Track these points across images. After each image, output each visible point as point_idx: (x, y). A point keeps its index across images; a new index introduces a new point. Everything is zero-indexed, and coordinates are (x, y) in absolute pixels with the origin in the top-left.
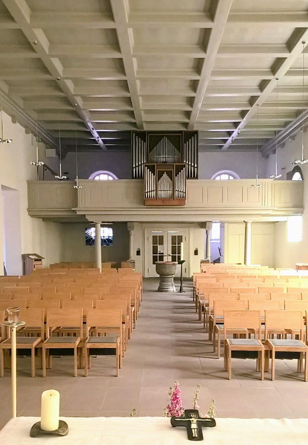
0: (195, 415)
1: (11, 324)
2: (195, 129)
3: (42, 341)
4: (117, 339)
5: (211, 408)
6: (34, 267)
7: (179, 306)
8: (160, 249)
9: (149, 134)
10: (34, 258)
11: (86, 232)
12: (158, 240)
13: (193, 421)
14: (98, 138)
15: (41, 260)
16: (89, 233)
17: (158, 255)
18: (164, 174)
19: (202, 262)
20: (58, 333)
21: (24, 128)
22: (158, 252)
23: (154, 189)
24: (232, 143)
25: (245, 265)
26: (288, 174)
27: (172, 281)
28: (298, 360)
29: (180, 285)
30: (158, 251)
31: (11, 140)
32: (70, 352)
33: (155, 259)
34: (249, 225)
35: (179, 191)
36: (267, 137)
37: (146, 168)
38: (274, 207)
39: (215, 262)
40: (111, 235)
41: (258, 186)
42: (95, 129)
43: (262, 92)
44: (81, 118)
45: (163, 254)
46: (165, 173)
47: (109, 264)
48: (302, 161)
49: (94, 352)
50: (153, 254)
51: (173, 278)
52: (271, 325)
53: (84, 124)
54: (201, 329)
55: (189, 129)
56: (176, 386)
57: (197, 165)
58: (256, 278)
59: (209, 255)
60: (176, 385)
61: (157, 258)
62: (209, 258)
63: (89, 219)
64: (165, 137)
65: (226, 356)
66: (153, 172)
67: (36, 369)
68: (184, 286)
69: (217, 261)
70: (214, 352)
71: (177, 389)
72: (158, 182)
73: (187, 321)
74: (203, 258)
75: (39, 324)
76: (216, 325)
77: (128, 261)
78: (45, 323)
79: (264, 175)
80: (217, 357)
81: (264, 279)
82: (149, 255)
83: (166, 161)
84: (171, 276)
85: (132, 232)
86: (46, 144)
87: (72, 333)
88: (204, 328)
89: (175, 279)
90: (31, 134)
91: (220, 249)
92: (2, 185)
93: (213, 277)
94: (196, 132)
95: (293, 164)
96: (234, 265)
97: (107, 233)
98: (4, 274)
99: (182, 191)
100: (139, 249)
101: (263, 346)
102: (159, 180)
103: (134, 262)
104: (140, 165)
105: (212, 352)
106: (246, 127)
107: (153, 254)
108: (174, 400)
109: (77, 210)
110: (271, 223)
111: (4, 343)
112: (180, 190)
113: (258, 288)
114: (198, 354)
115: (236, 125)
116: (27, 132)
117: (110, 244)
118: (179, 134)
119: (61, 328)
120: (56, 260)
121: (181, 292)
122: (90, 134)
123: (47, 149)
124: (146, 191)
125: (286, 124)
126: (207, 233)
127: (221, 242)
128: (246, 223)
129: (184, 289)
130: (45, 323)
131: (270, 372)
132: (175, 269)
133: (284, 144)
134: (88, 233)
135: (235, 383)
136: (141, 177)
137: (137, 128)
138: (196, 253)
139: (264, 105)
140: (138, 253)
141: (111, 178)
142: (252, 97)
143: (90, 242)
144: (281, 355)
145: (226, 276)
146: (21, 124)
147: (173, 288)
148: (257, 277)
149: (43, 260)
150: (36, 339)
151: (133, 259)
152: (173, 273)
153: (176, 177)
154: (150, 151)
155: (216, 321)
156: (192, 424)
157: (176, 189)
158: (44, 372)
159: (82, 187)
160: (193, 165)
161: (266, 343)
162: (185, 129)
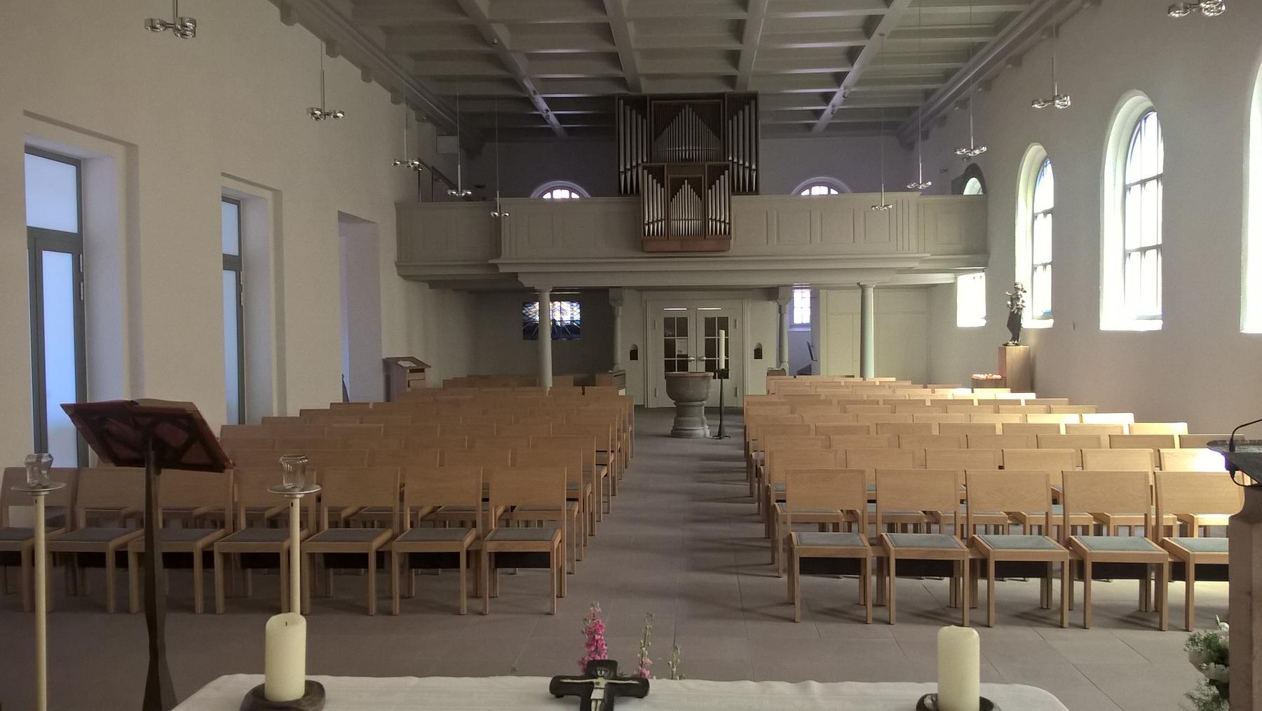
0: (606, 671)
1: (289, 490)
2: (751, 88)
3: (393, 537)
4: (555, 532)
5: (671, 663)
6: (409, 386)
7: (710, 467)
8: (679, 346)
9: (652, 102)
10: (408, 366)
11: (524, 311)
12: (677, 327)
13: (598, 683)
14: (547, 111)
15: (422, 371)
16: (530, 313)
17: (676, 359)
18: (684, 184)
19: (771, 373)
20: (436, 519)
21: (389, 91)
22: (677, 354)
23: (663, 218)
24: (833, 119)
25: (862, 378)
26: (953, 182)
27: (701, 413)
28: (950, 580)
29: (719, 422)
31: (343, 113)
32: (449, 561)
33: (669, 366)
34: (871, 294)
35: (720, 221)
36: (908, 104)
37: (646, 172)
38: (924, 253)
39: (802, 372)
40: (577, 317)
41: (885, 208)
42: (540, 94)
43: (888, 7)
45: (687, 356)
46: (686, 181)
47: (570, 379)
48: (972, 150)
49: (504, 560)
50: (665, 357)
51: (703, 408)
52: (890, 504)
53: (514, 83)
54: (752, 515)
55: (739, 90)
56: (594, 614)
57: (756, 166)
58: (878, 404)
59: (786, 357)
60: (592, 611)
61: (675, 364)
62: (786, 366)
63: (527, 282)
64: (687, 106)
65: (790, 571)
66: (661, 181)
67: (379, 598)
68: (727, 426)
69: (807, 371)
70: (772, 564)
71: (595, 621)
72: (671, 201)
73: (725, 499)
74: (773, 365)
75: (386, 499)
76: (776, 504)
77: (610, 371)
78: (402, 499)
79: (900, 183)
80: (777, 575)
81: (894, 405)
82: (656, 358)
83: (687, 157)
84: (699, 403)
85: (620, 311)
86: (435, 123)
87: (464, 521)
88: (758, 514)
89: (709, 411)
90: (404, 105)
91: (811, 345)
92: (339, 212)
93: (783, 404)
94: (754, 97)
95: (965, 160)
96: (837, 380)
97: (567, 312)
98: (342, 398)
99: (722, 220)
100: (635, 345)
101: (870, 548)
102: (673, 197)
103: (625, 374)
104: (634, 167)
105: (769, 564)
106: (859, 83)
107: (665, 357)
108: (591, 645)
109: (501, 264)
110: (911, 288)
111: (311, 541)
112: (718, 218)
113: (877, 424)
114: (737, 567)
115: (839, 78)
116: (395, 101)
117: (574, 335)
118: (718, 100)
119: (441, 508)
120: (459, 370)
121: (720, 439)
122: (529, 102)
123: (440, 135)
124: (646, 222)
125: (948, 75)
126: (780, 312)
127: (812, 331)
128: (863, 288)
129: (727, 430)
130: (402, 499)
131: (888, 604)
132: (708, 388)
133: (945, 118)
134: (527, 314)
135: (810, 630)
136: (634, 192)
137: (628, 89)
138: (758, 354)
139: (896, 34)
140: (634, 355)
141: (575, 196)
142: (870, 17)
143: (531, 331)
144: (910, 568)
145: (814, 400)
146: (380, 83)
147: (704, 430)
148: (881, 403)
149: (426, 370)
150: (379, 534)
151: (621, 368)
152: (704, 396)
153: (710, 191)
154: (656, 137)
155: (777, 495)
156: (595, 691)
157: (710, 217)
158: (396, 604)
159: (507, 214)
160: (747, 164)
161: (878, 542)
162: (731, 90)
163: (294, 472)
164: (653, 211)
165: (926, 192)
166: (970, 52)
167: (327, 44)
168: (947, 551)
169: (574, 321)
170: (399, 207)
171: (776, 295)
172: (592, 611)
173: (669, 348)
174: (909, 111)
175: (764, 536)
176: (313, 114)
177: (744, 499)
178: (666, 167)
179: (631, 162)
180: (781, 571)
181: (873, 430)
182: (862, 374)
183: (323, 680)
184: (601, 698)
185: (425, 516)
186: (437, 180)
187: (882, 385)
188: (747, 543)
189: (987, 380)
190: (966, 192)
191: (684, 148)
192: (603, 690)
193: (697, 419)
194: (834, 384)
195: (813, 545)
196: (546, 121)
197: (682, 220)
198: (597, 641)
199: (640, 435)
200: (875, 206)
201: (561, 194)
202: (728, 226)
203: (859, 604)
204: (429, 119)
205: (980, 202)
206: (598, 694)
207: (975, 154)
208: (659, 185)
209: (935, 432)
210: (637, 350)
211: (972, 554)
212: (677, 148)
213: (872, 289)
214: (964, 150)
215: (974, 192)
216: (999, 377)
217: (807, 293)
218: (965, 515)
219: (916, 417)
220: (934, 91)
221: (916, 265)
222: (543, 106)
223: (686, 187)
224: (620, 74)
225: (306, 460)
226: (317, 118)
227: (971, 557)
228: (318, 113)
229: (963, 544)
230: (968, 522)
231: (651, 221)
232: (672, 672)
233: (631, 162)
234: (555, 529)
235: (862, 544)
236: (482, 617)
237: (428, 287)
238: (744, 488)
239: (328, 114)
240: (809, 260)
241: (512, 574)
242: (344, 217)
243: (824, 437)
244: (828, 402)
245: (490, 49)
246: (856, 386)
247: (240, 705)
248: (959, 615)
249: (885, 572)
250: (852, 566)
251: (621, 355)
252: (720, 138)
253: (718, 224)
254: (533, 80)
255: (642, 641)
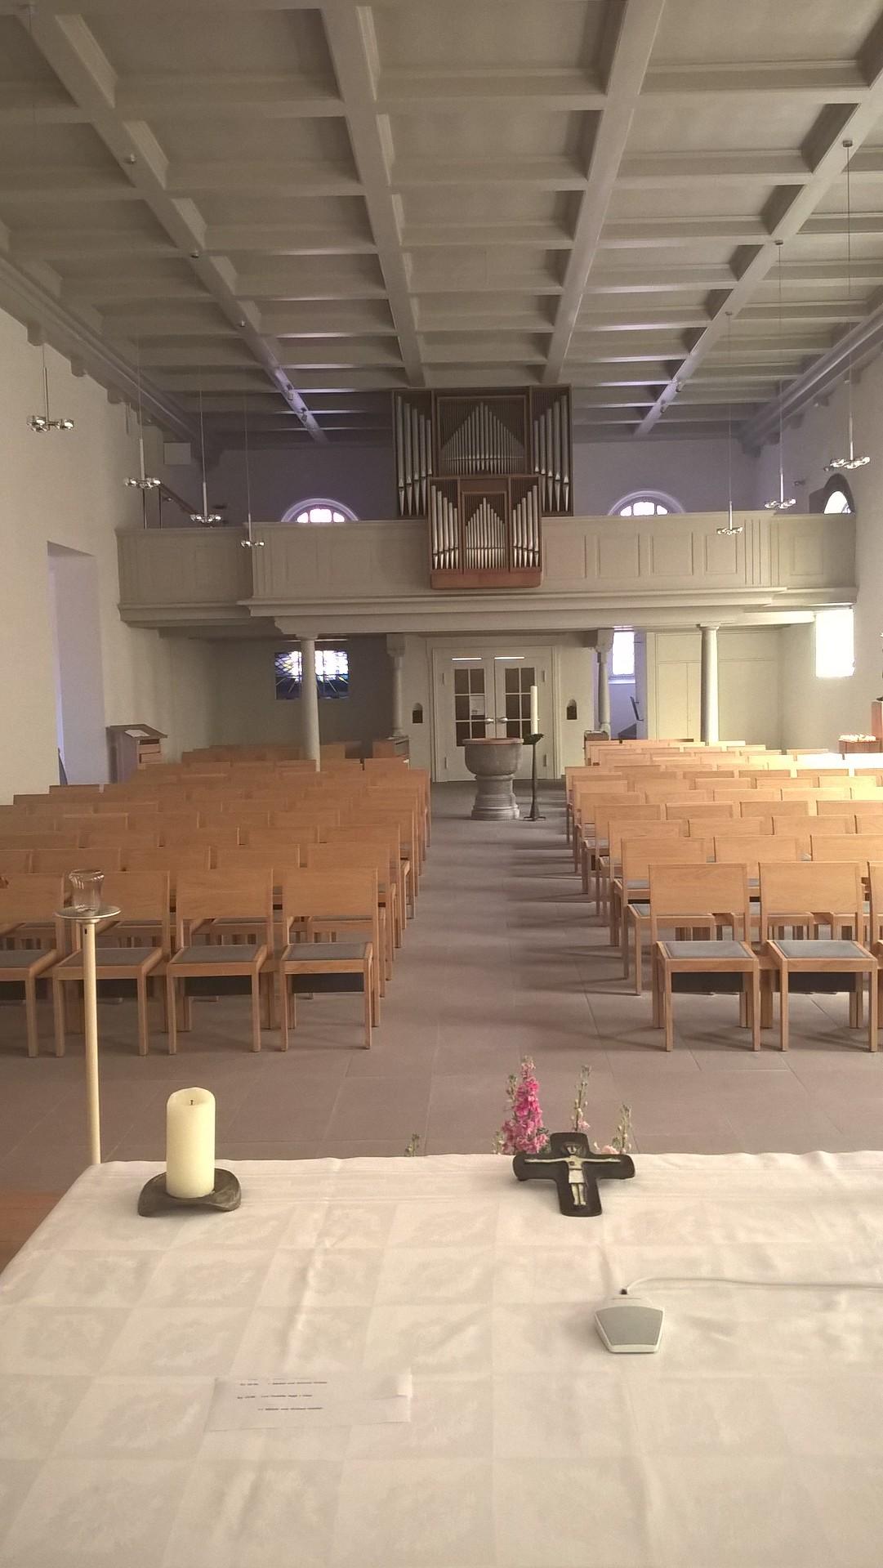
1: (81, 914)
2: (562, 381)
5: (620, 1128)
7: (528, 856)
9: (439, 399)
11: (277, 664)
12: (470, 682)
13: (572, 1163)
15: (157, 741)
16: (285, 665)
19: (588, 737)
20: (208, 934)
23: (456, 546)
24: (660, 418)
30: (471, 708)
31: (72, 422)
32: (241, 985)
33: (462, 733)
34: (713, 637)
37: (434, 487)
40: (344, 670)
41: (734, 531)
44: (255, 359)
45: (483, 717)
46: (485, 500)
47: (341, 748)
48: (851, 462)
49: (304, 984)
52: (776, 902)
53: (266, 376)
55: (547, 383)
57: (569, 478)
59: (607, 718)
60: (525, 1068)
61: (469, 729)
62: (607, 728)
63: (286, 628)
64: (482, 404)
66: (453, 500)
69: (630, 734)
75: (156, 912)
76: (630, 906)
77: (390, 738)
78: (173, 909)
79: (750, 501)
80: (634, 992)
81: (756, 778)
82: (445, 723)
84: (506, 777)
85: (401, 662)
86: (160, 425)
87: (245, 934)
89: (519, 785)
90: (123, 404)
92: (49, 542)
93: (618, 778)
94: (566, 391)
97: (332, 664)
100: (419, 704)
105: (621, 979)
106: (697, 373)
108: (523, 1109)
109: (252, 606)
110: (760, 629)
111: (64, 965)
113: (741, 803)
115: (671, 368)
116: (113, 400)
117: (341, 693)
120: (198, 740)
121: (533, 820)
122: (281, 400)
124: (435, 551)
125: (805, 363)
126: (599, 661)
128: (704, 631)
129: (541, 809)
130: (173, 909)
132: (517, 759)
133: (801, 417)
134: (280, 667)
136: (420, 513)
137: (407, 381)
138: (572, 713)
139: (746, 313)
140: (418, 717)
143: (289, 689)
144: (804, 982)
147: (513, 811)
148: (736, 774)
152: (512, 768)
153: (514, 511)
154: (443, 443)
155: (630, 894)
157: (515, 544)
158: (173, 1039)
159: (262, 544)
161: (764, 951)
162: (536, 383)
163: (88, 890)
164: (444, 537)
165: (791, 510)
166: (835, 334)
167: (29, 328)
168: (851, 962)
169: (340, 675)
170: (122, 535)
171: (593, 639)
172: (525, 1068)
173: (462, 708)
174: (755, 407)
175: (609, 944)
176: (35, 424)
177: (576, 897)
178: (459, 482)
179: (413, 472)
180: (639, 985)
181: (736, 810)
182: (704, 738)
183: (238, 1168)
184: (582, 1181)
185: (197, 929)
186: (166, 499)
187: (730, 752)
188: (596, 953)
189: (859, 742)
190: (826, 512)
191: (478, 457)
192: (581, 1172)
193: (504, 796)
194: (671, 751)
195: (687, 958)
196: (302, 424)
197: (481, 549)
198: (531, 1104)
199: (436, 818)
200: (721, 529)
201: (321, 516)
202: (537, 556)
203: (740, 1027)
204: (156, 422)
205: (845, 525)
206: (576, 1177)
207: (854, 466)
208: (451, 504)
209: (813, 812)
210: (421, 712)
211: (880, 965)
212: (470, 457)
213: (715, 631)
214: (843, 461)
215: (838, 510)
216: (873, 739)
217: (631, 636)
218: (868, 915)
219: (786, 792)
220: (788, 383)
221: (769, 601)
222: (299, 403)
223: (485, 506)
224: (397, 363)
225: (102, 876)
226: (39, 429)
227: (879, 968)
228: (41, 422)
229: (866, 951)
230: (856, 922)
231: (441, 550)
232: (624, 1138)
233: (413, 472)
234: (366, 943)
235: (746, 955)
236: (279, 1055)
237: (158, 635)
238: (577, 883)
239: (54, 424)
240: (620, 597)
241: (309, 999)
242: (54, 549)
243: (680, 821)
244: (669, 775)
245: (234, 333)
246: (701, 753)
247: (138, 1198)
248: (865, 1037)
249: (773, 986)
250: (731, 981)
251: (403, 716)
252: (523, 444)
253: (526, 553)
254: (287, 372)
255: (577, 1101)
